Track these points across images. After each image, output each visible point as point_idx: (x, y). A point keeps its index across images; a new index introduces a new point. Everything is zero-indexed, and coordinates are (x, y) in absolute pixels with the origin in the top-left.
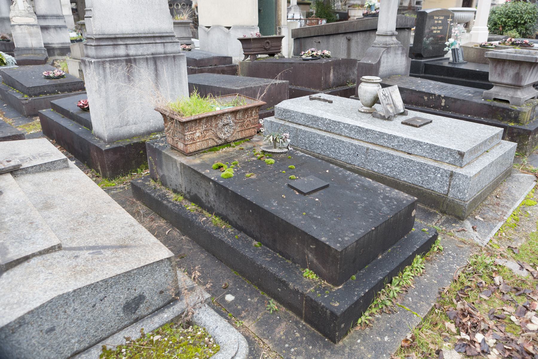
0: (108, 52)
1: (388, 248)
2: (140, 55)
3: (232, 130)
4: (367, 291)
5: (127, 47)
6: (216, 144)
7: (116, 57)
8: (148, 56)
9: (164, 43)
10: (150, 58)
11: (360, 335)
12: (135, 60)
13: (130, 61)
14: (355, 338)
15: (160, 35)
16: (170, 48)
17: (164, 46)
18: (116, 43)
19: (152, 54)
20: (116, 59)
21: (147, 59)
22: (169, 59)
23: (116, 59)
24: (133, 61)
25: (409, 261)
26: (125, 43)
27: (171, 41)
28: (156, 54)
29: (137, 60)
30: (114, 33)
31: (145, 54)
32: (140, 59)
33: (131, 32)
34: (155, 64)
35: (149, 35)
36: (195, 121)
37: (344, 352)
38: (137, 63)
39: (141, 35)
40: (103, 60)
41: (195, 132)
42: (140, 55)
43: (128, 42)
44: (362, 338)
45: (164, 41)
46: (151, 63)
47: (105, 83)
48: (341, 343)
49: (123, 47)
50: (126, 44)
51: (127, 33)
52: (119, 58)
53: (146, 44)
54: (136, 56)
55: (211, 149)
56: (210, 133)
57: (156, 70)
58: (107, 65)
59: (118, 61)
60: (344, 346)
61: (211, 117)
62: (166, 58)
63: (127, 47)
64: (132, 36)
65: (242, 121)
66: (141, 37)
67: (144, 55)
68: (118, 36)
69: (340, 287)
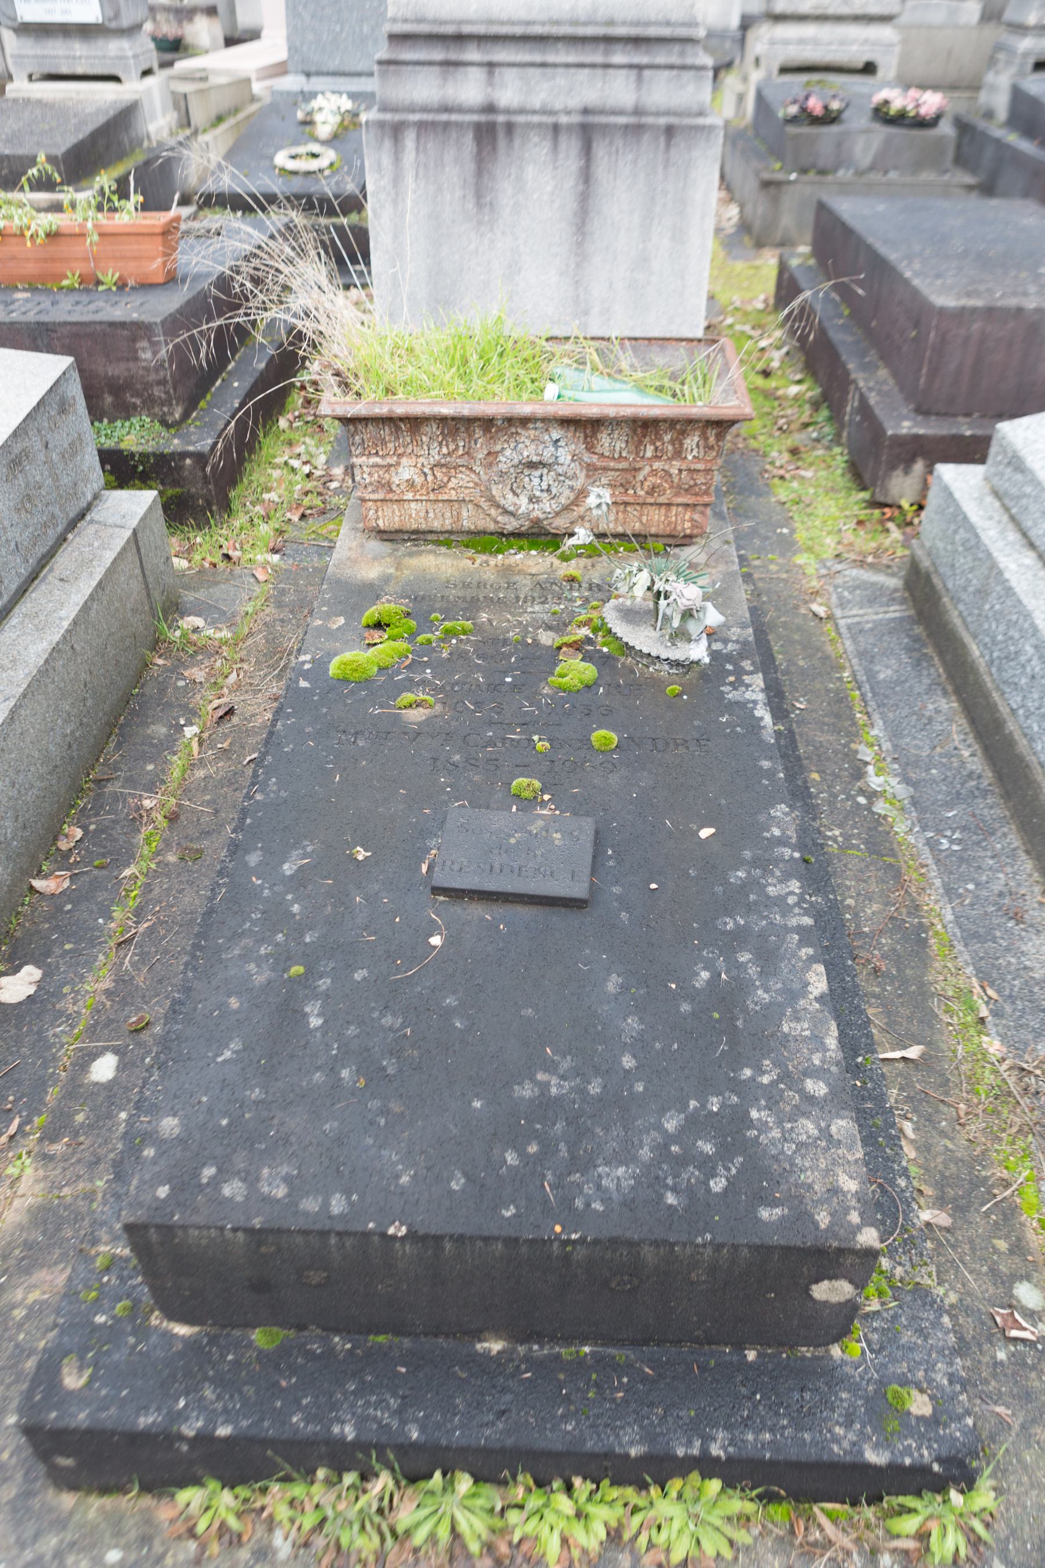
0: (423, 88)
1: (584, 1340)
2: (534, 112)
3: (567, 492)
4: (224, 1431)
5: (491, 74)
6: (492, 527)
7: (447, 109)
8: (564, 119)
9: (640, 68)
10: (570, 127)
11: (146, 1540)
12: (510, 127)
13: (490, 133)
14: (118, 1534)
15: (633, 31)
16: (665, 93)
17: (639, 79)
18: (453, 56)
19: (586, 111)
20: (444, 117)
21: (556, 128)
22: (646, 137)
23: (444, 117)
24: (501, 134)
25: (654, 1471)
26: (487, 58)
27: (674, 59)
28: (602, 112)
29: (518, 133)
30: (459, 15)
31: (558, 105)
32: (529, 126)
33: (522, 15)
34: (587, 151)
35: (589, 31)
36: (390, 421)
37: (36, 1537)
38: (517, 142)
39: (555, 30)
40: (398, 117)
41: (392, 460)
42: (534, 112)
43: (501, 54)
44: (133, 1557)
45: (644, 60)
46: (570, 146)
47: (395, 202)
48: (68, 1500)
49: (476, 75)
50: (491, 66)
51: (504, 16)
52: (454, 117)
53: (567, 66)
54: (522, 111)
55: (482, 541)
56: (463, 478)
57: (586, 176)
58: (410, 140)
59: (447, 125)
60: (61, 1523)
61: (469, 421)
62: (635, 131)
63: (491, 74)
64: (518, 30)
65: (623, 465)
66: (558, 39)
67: (551, 113)
68: (466, 29)
69: (182, 1330)
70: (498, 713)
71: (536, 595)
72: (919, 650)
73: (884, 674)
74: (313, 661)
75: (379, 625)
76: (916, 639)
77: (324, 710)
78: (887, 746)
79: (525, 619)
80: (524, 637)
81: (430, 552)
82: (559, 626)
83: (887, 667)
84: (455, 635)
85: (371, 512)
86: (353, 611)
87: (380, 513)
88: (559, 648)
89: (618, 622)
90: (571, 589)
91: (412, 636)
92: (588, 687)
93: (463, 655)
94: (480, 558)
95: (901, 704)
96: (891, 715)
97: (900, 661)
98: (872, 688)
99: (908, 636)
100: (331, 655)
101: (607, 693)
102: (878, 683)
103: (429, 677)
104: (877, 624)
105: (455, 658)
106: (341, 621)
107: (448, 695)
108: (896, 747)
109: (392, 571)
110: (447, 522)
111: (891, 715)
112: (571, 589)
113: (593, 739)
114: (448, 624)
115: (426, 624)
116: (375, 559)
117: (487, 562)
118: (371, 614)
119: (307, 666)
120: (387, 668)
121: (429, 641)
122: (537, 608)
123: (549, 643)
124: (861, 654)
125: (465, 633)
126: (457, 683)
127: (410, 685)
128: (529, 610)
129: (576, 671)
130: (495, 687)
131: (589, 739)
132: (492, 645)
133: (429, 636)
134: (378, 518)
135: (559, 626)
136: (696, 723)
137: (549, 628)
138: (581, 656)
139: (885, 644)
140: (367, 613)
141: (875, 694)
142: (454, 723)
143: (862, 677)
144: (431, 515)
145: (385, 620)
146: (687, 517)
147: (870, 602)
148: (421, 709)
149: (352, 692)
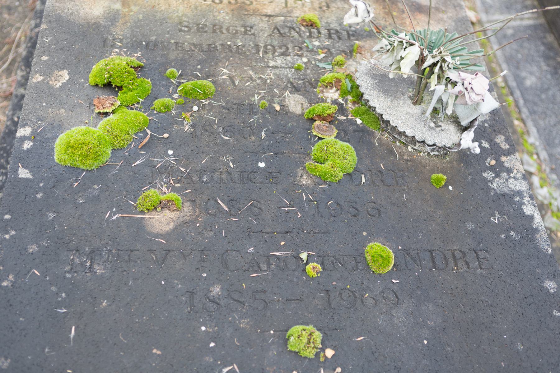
70: (256, 216)
71: (275, 43)
72: (554, 59)
73: (530, 81)
74: (33, 137)
75: (109, 87)
76: (550, 47)
77: (51, 215)
78: (544, 155)
79: (269, 75)
80: (271, 102)
82: (307, 87)
83: (531, 73)
84: (196, 101)
86: (78, 64)
88: (312, 120)
89: (375, 93)
90: (310, 36)
91: (150, 98)
92: (349, 175)
93: (207, 127)
95: (549, 113)
96: (541, 123)
97: (540, 67)
98: (522, 94)
99: (544, 44)
100: (57, 128)
101: (371, 183)
102: (526, 89)
103: (172, 161)
104: (517, 29)
105: (199, 131)
106: (65, 76)
107: (194, 186)
108: (551, 155)
111: (541, 123)
112: (310, 36)
113: (367, 249)
114: (189, 85)
115: (163, 85)
118: (98, 70)
119: (27, 145)
120: (122, 149)
121: (167, 108)
122: (279, 61)
123: (298, 111)
124: (509, 60)
125: (206, 97)
126: (204, 171)
127: (151, 175)
128: (272, 63)
129: (336, 155)
130: (248, 176)
131: (362, 255)
132: (239, 111)
133: (167, 100)
135: (307, 87)
136: (470, 226)
137: (296, 89)
138: (335, 132)
139: (526, 51)
140: (95, 68)
141: (525, 101)
142: (208, 234)
143: (513, 84)
145: (116, 82)
147: (507, 8)
148: (166, 212)
149: (84, 187)
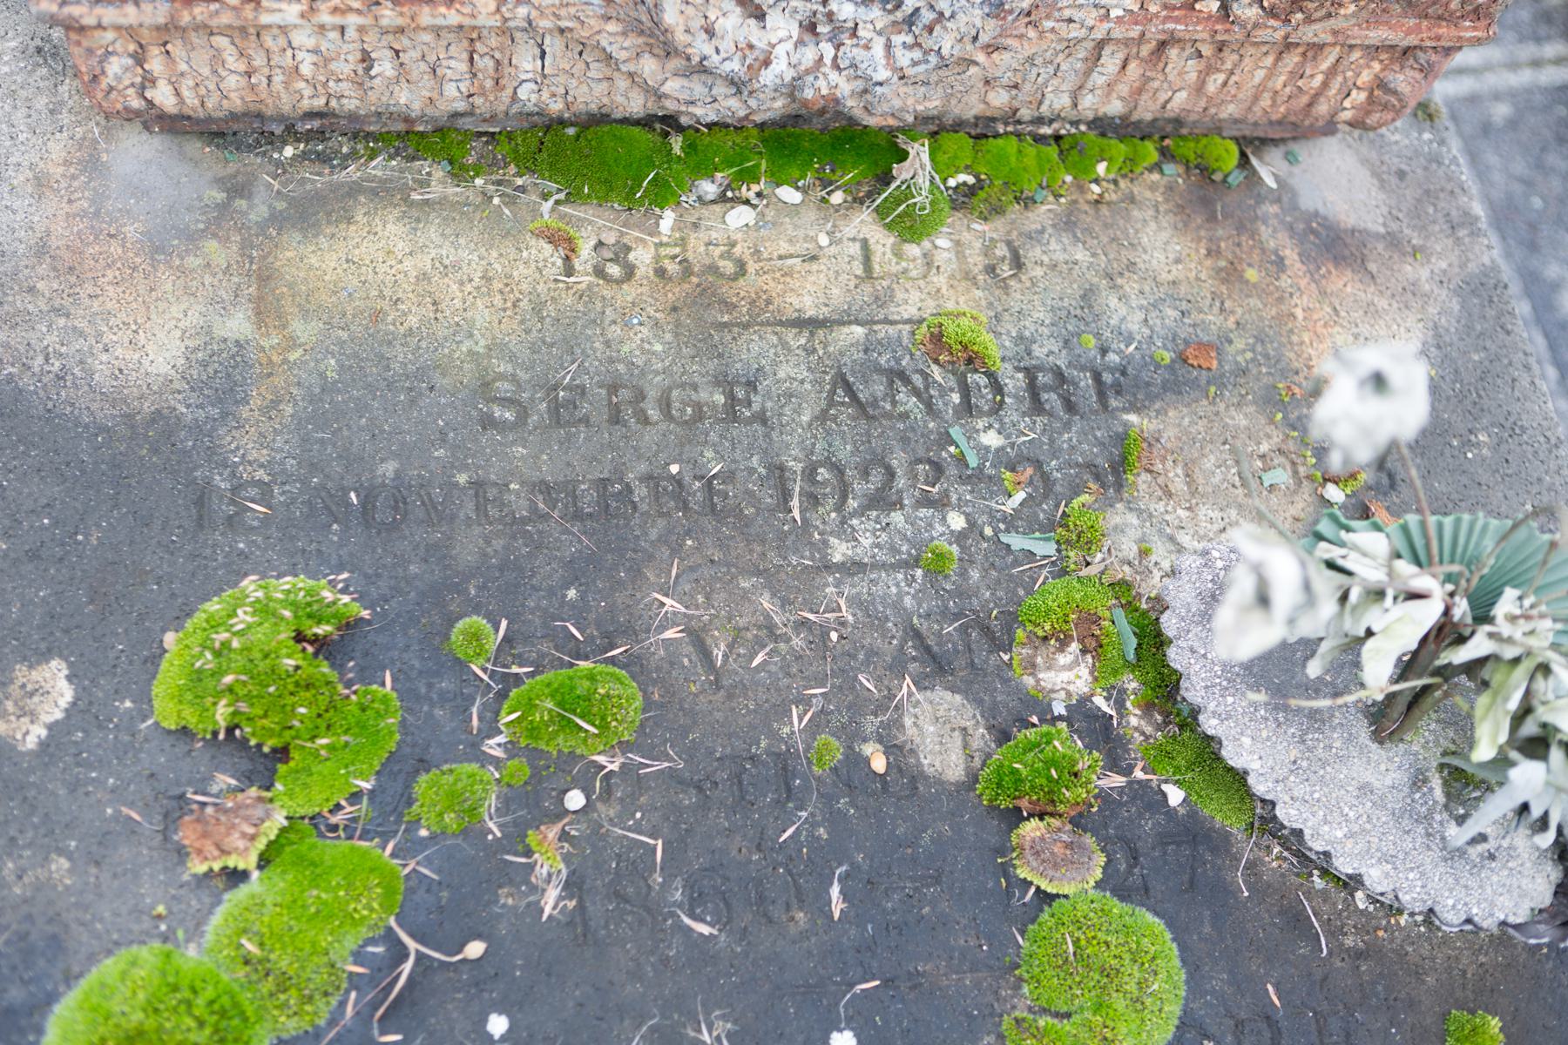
6: (636, 105)
81: (381, 192)
85: (115, 67)
87: (156, 64)
94: (595, 226)
104: (1523, 100)
109: (238, 325)
110: (451, 90)
116: (156, 250)
117: (621, 253)
134: (149, 80)
144: (384, 67)
146: (1365, 77)
